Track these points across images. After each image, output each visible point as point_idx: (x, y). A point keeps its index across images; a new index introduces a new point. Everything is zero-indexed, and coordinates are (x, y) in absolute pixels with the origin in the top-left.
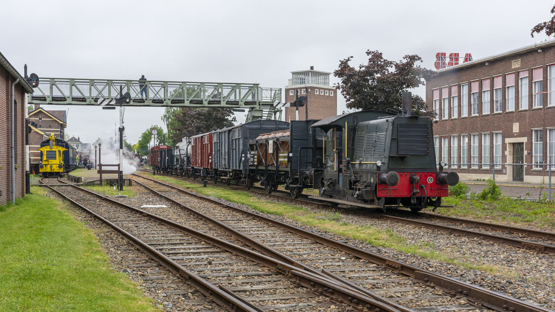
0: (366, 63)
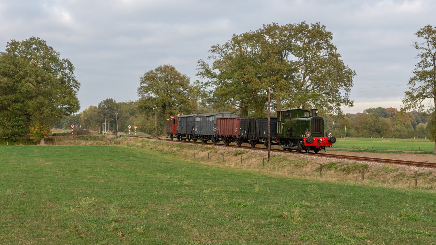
0: (432, 70)
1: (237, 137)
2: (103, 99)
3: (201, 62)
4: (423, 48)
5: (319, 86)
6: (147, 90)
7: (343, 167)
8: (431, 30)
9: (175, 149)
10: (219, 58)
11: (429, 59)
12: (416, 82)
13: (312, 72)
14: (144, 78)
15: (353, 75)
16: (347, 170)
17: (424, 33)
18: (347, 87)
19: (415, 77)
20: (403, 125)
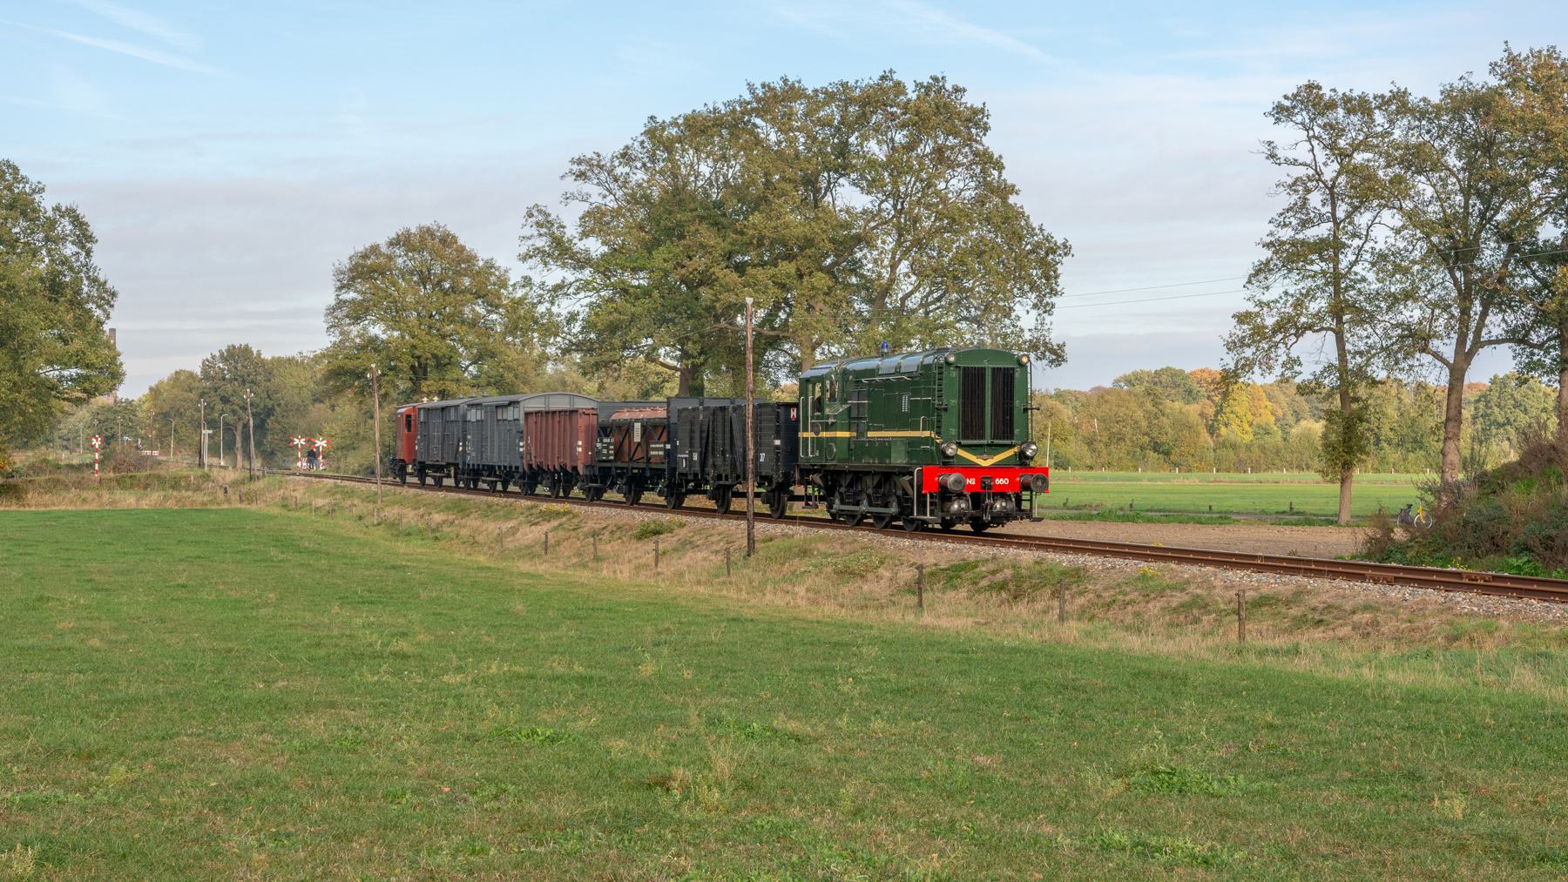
0: (1325, 236)
1: (581, 470)
2: (219, 344)
3: (536, 214)
4: (1295, 163)
5: (944, 294)
6: (358, 313)
7: (999, 577)
8: (1321, 97)
9: (437, 518)
10: (600, 200)
11: (1316, 199)
12: (1271, 278)
13: (919, 244)
14: (351, 270)
15: (1060, 255)
16: (1011, 586)
17: (1296, 111)
18: (1041, 298)
19: (1268, 262)
20: (1246, 426)
